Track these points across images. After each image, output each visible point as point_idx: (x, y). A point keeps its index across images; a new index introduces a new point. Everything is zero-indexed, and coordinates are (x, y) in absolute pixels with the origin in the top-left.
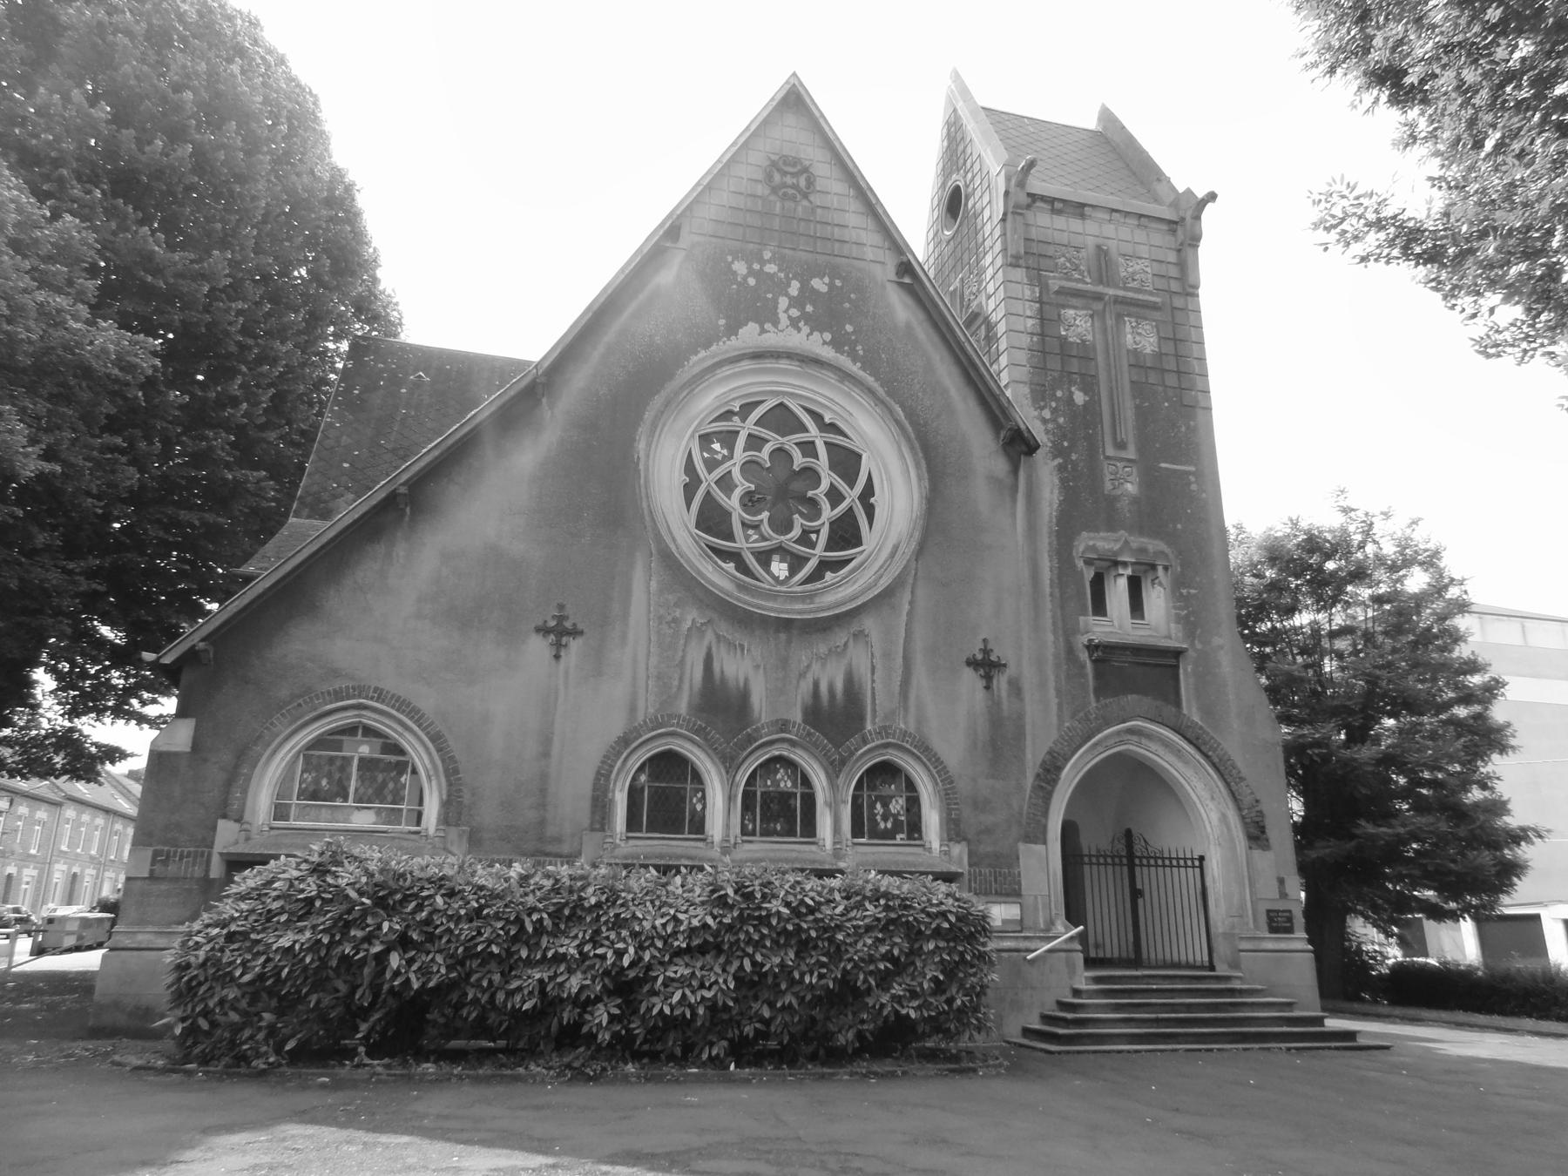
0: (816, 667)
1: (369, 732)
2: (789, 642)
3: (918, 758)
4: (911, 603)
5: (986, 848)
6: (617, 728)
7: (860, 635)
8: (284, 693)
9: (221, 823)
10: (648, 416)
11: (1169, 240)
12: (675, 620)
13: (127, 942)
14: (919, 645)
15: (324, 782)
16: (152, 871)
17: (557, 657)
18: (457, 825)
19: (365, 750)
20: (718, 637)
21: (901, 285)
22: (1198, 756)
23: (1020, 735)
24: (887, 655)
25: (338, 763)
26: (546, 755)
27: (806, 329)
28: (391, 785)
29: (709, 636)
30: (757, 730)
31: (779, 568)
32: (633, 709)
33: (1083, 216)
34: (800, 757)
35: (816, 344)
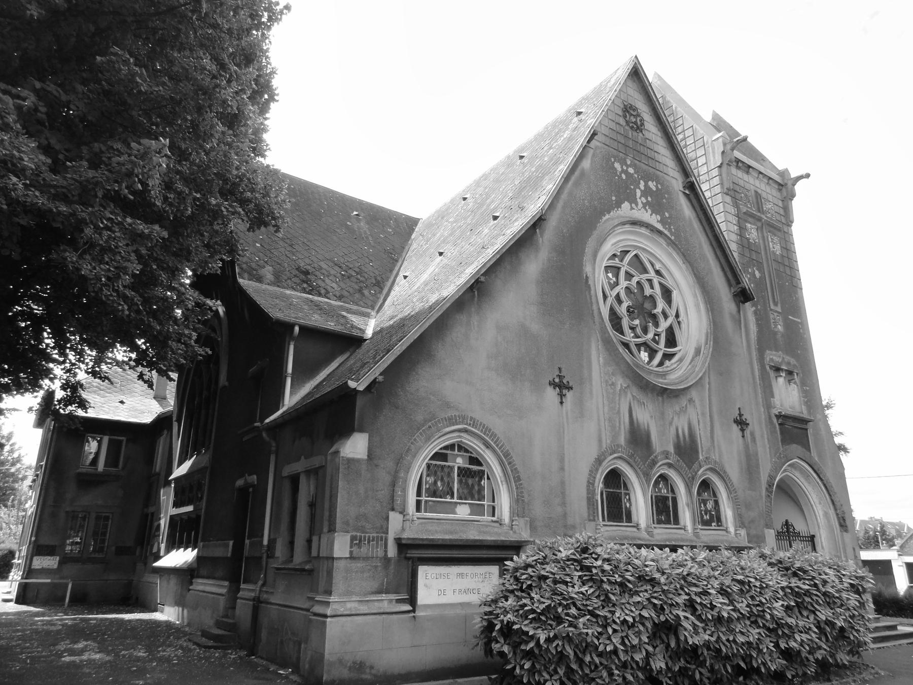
0: (676, 419)
1: (461, 448)
2: (663, 402)
3: (632, 466)
4: (709, 383)
5: (753, 532)
6: (594, 453)
7: (691, 401)
8: (420, 418)
9: (392, 515)
10: (589, 250)
11: (777, 194)
12: (613, 384)
13: (341, 610)
14: (715, 409)
15: (439, 484)
16: (351, 552)
17: (562, 403)
18: (523, 517)
19: (460, 461)
20: (633, 396)
21: (684, 193)
22: (818, 480)
23: (758, 466)
24: (703, 414)
25: (446, 470)
26: (562, 469)
27: (650, 211)
28: (476, 488)
29: (629, 395)
30: (656, 457)
31: (644, 356)
32: (600, 441)
33: (748, 173)
34: (672, 474)
35: (653, 220)
